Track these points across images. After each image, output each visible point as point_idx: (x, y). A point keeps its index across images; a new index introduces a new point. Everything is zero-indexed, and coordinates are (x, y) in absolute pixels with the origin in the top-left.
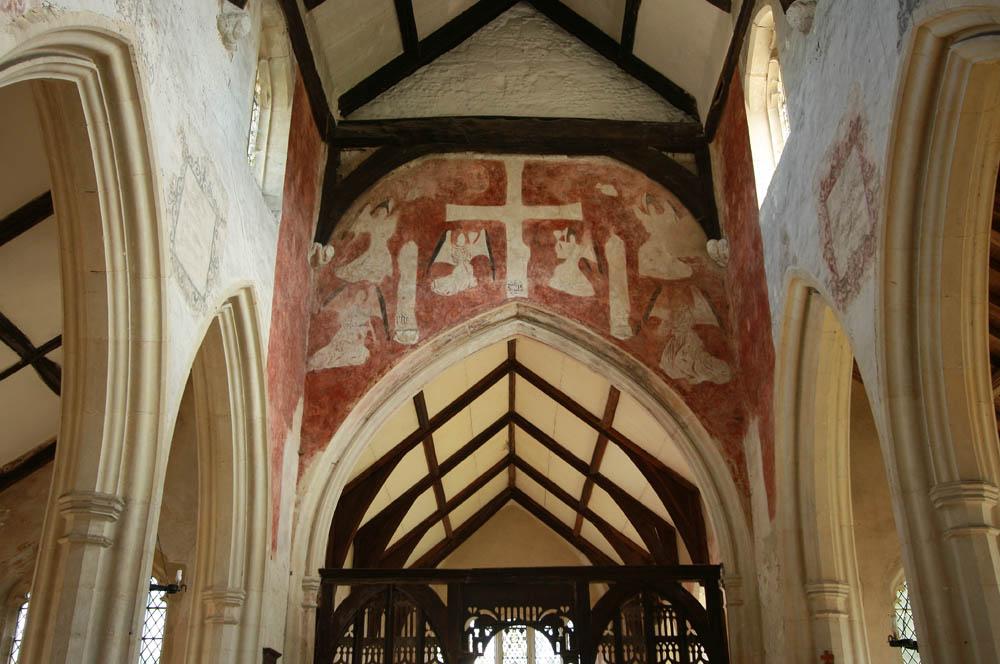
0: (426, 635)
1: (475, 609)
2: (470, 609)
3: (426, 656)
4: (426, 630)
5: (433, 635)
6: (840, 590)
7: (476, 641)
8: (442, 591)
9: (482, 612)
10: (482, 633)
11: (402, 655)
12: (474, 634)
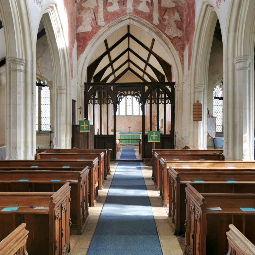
5: (168, 97)
7: (119, 99)
11: (96, 102)
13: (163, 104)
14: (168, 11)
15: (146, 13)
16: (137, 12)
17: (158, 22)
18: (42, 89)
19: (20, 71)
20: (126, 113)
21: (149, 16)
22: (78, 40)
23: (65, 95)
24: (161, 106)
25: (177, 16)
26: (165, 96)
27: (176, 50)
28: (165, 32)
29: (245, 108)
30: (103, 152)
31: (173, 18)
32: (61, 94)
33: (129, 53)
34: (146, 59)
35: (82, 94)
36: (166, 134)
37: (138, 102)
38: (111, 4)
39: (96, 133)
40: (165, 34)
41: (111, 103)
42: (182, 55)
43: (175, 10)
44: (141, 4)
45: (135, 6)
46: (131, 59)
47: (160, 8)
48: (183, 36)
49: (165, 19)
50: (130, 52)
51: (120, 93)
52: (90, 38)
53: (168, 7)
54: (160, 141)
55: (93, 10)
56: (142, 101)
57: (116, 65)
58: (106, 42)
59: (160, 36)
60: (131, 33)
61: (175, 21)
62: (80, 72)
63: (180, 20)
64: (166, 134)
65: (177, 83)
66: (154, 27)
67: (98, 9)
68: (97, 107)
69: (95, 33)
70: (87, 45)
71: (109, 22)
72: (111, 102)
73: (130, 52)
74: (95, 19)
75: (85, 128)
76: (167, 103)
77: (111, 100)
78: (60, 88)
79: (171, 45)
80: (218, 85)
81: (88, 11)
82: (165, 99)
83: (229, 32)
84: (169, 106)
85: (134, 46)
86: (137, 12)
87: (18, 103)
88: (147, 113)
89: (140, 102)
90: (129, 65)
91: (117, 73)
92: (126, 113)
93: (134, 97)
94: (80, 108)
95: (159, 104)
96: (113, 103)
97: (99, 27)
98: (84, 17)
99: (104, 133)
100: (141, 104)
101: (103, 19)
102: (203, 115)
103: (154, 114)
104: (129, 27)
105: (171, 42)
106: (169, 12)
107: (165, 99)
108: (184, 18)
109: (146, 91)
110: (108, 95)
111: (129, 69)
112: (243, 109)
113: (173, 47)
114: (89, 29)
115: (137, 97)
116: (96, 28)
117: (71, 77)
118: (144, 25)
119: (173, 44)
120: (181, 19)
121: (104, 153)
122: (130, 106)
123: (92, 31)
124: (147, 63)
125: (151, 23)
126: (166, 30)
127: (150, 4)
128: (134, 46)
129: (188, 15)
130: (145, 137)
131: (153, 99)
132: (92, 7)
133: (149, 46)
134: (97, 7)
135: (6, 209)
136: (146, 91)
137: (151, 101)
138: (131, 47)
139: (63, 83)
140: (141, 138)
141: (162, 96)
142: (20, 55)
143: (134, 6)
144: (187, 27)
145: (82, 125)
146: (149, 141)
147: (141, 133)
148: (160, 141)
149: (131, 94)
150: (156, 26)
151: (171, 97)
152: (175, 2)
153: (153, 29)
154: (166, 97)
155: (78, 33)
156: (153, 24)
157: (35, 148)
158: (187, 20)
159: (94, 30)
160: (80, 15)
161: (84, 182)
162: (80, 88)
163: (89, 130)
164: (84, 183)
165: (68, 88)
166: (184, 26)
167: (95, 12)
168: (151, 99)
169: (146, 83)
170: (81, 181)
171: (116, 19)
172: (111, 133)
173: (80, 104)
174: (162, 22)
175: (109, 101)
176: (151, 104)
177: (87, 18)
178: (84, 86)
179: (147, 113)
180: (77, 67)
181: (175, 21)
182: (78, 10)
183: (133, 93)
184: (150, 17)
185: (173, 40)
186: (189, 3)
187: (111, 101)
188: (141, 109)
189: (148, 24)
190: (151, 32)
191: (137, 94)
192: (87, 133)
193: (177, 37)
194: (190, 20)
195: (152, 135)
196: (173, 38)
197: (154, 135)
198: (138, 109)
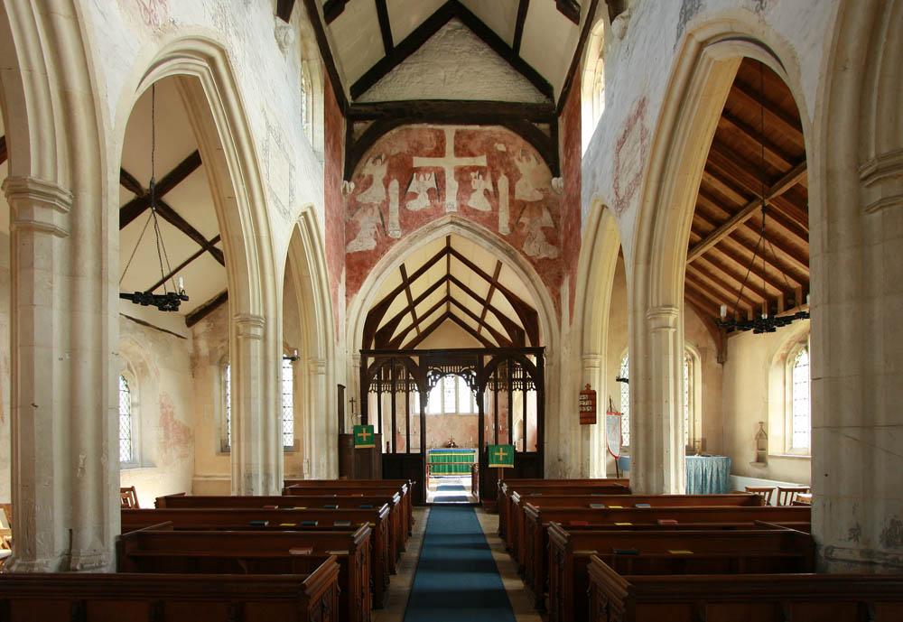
7: (432, 381)
8: (416, 359)
10: (435, 378)
13: (521, 392)
14: (528, 207)
15: (484, 213)
16: (465, 211)
17: (508, 230)
19: (256, 337)
20: (443, 408)
21: (489, 218)
22: (349, 267)
23: (58, 243)
24: (517, 395)
25: (546, 218)
26: (525, 375)
27: (546, 285)
28: (524, 249)
31: (538, 221)
32: (250, 338)
33: (448, 283)
34: (484, 297)
35: (355, 372)
36: (528, 450)
37: (469, 388)
38: (414, 196)
39: (384, 451)
40: (523, 253)
42: (556, 294)
43: (543, 206)
44: (473, 195)
45: (462, 199)
46: (452, 295)
47: (512, 202)
48: (559, 258)
49: (523, 224)
50: (451, 283)
52: (373, 263)
53: (529, 200)
54: (512, 466)
55: (379, 208)
56: (478, 386)
57: (421, 310)
58: (402, 268)
59: (513, 257)
60: (453, 246)
61: (543, 228)
62: (351, 330)
63: (553, 226)
64: (528, 450)
65: (548, 349)
66: (500, 241)
67: (388, 207)
68: (386, 397)
69: (383, 253)
70: (365, 277)
71: (411, 230)
73: (452, 283)
74: (383, 227)
75: (365, 440)
76: (530, 389)
78: (316, 362)
79: (535, 275)
81: (370, 211)
82: (524, 380)
83: (636, 263)
84: (532, 396)
85: (457, 293)
86: (465, 211)
87: (252, 396)
88: (488, 410)
89: (473, 388)
90: (448, 308)
91: (423, 326)
92: (443, 408)
93: (460, 377)
94: (352, 401)
96: (419, 391)
97: (391, 242)
98: (362, 222)
99: (401, 450)
100: (476, 392)
101: (398, 225)
102: (600, 413)
103: (502, 410)
104: (448, 238)
105: (536, 269)
106: (531, 210)
107: (524, 380)
108: (562, 221)
109: (485, 364)
111: (449, 314)
113: (539, 277)
114: (370, 244)
115: (468, 377)
116: (385, 242)
117: (335, 340)
118: (480, 234)
119: (539, 273)
120: (555, 224)
122: (451, 398)
123: (377, 249)
124: (486, 305)
125: (494, 232)
126: (525, 245)
127: (492, 194)
128: (457, 293)
129: (568, 218)
130: (484, 457)
131: (500, 380)
132: (376, 202)
133: (490, 273)
134: (387, 202)
135: (295, 552)
136: (485, 364)
137: (496, 386)
138: (452, 273)
139: (321, 355)
140: (476, 461)
141: (519, 375)
142: (255, 309)
143: (459, 198)
144: (566, 241)
145: (359, 435)
146: (490, 466)
147: (477, 450)
148: (512, 466)
150: (503, 237)
151: (537, 377)
152: (541, 190)
153: (499, 243)
155: (349, 254)
156: (498, 234)
157: (282, 479)
158: (566, 226)
159: (381, 247)
160: (352, 219)
161: (362, 555)
162: (352, 361)
163: (373, 443)
164: (362, 558)
165: (331, 362)
166: (562, 238)
167: (384, 212)
168: (496, 381)
169: (489, 348)
170: (356, 553)
171: (423, 224)
172: (415, 450)
173: (352, 392)
174: (516, 229)
176: (496, 391)
177: (367, 224)
178: (360, 357)
179: (488, 410)
180: (347, 320)
181: (543, 228)
182: (349, 208)
184: (492, 220)
185: (540, 265)
186: (569, 195)
188: (475, 402)
189: (488, 233)
190: (494, 248)
191: (468, 372)
192: (370, 449)
193: (548, 259)
194: (573, 228)
195: (497, 454)
196: (539, 261)
197: (501, 454)
198: (469, 400)
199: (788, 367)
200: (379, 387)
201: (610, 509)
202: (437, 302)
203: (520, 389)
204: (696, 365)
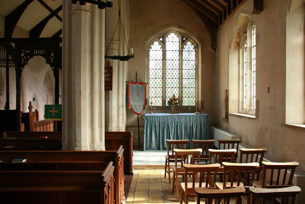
0: (9, 58)
1: (24, 51)
2: (23, 51)
3: (9, 65)
4: (9, 57)
5: (11, 58)
6: (114, 43)
7: (24, 60)
8: (13, 45)
9: (27, 51)
10: (26, 58)
11: (11, 64)
12: (24, 58)
18: (151, 48)
26: (8, 56)
29: (78, 71)
30: (122, 146)
41: (12, 67)
51: (25, 52)
72: (12, 65)
77: (13, 63)
80: (189, 41)
95: (9, 67)
110: (9, 55)
112: (77, 71)
121: (123, 148)
149: (40, 54)
154: (9, 58)
175: (10, 63)
183: (43, 52)
187: (12, 63)
195: (50, 111)
199: (241, 51)
200: (8, 64)
201: (13, 163)
202: (44, 8)
203: (4, 67)
204: (199, 50)
